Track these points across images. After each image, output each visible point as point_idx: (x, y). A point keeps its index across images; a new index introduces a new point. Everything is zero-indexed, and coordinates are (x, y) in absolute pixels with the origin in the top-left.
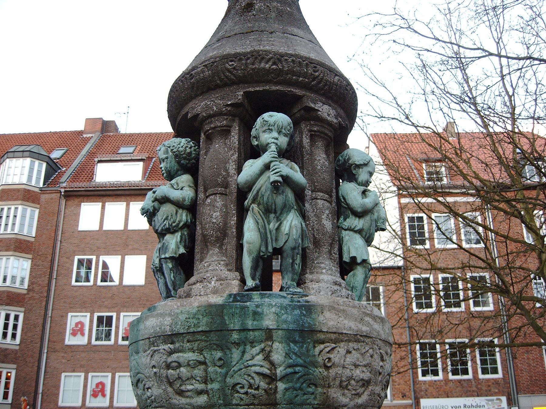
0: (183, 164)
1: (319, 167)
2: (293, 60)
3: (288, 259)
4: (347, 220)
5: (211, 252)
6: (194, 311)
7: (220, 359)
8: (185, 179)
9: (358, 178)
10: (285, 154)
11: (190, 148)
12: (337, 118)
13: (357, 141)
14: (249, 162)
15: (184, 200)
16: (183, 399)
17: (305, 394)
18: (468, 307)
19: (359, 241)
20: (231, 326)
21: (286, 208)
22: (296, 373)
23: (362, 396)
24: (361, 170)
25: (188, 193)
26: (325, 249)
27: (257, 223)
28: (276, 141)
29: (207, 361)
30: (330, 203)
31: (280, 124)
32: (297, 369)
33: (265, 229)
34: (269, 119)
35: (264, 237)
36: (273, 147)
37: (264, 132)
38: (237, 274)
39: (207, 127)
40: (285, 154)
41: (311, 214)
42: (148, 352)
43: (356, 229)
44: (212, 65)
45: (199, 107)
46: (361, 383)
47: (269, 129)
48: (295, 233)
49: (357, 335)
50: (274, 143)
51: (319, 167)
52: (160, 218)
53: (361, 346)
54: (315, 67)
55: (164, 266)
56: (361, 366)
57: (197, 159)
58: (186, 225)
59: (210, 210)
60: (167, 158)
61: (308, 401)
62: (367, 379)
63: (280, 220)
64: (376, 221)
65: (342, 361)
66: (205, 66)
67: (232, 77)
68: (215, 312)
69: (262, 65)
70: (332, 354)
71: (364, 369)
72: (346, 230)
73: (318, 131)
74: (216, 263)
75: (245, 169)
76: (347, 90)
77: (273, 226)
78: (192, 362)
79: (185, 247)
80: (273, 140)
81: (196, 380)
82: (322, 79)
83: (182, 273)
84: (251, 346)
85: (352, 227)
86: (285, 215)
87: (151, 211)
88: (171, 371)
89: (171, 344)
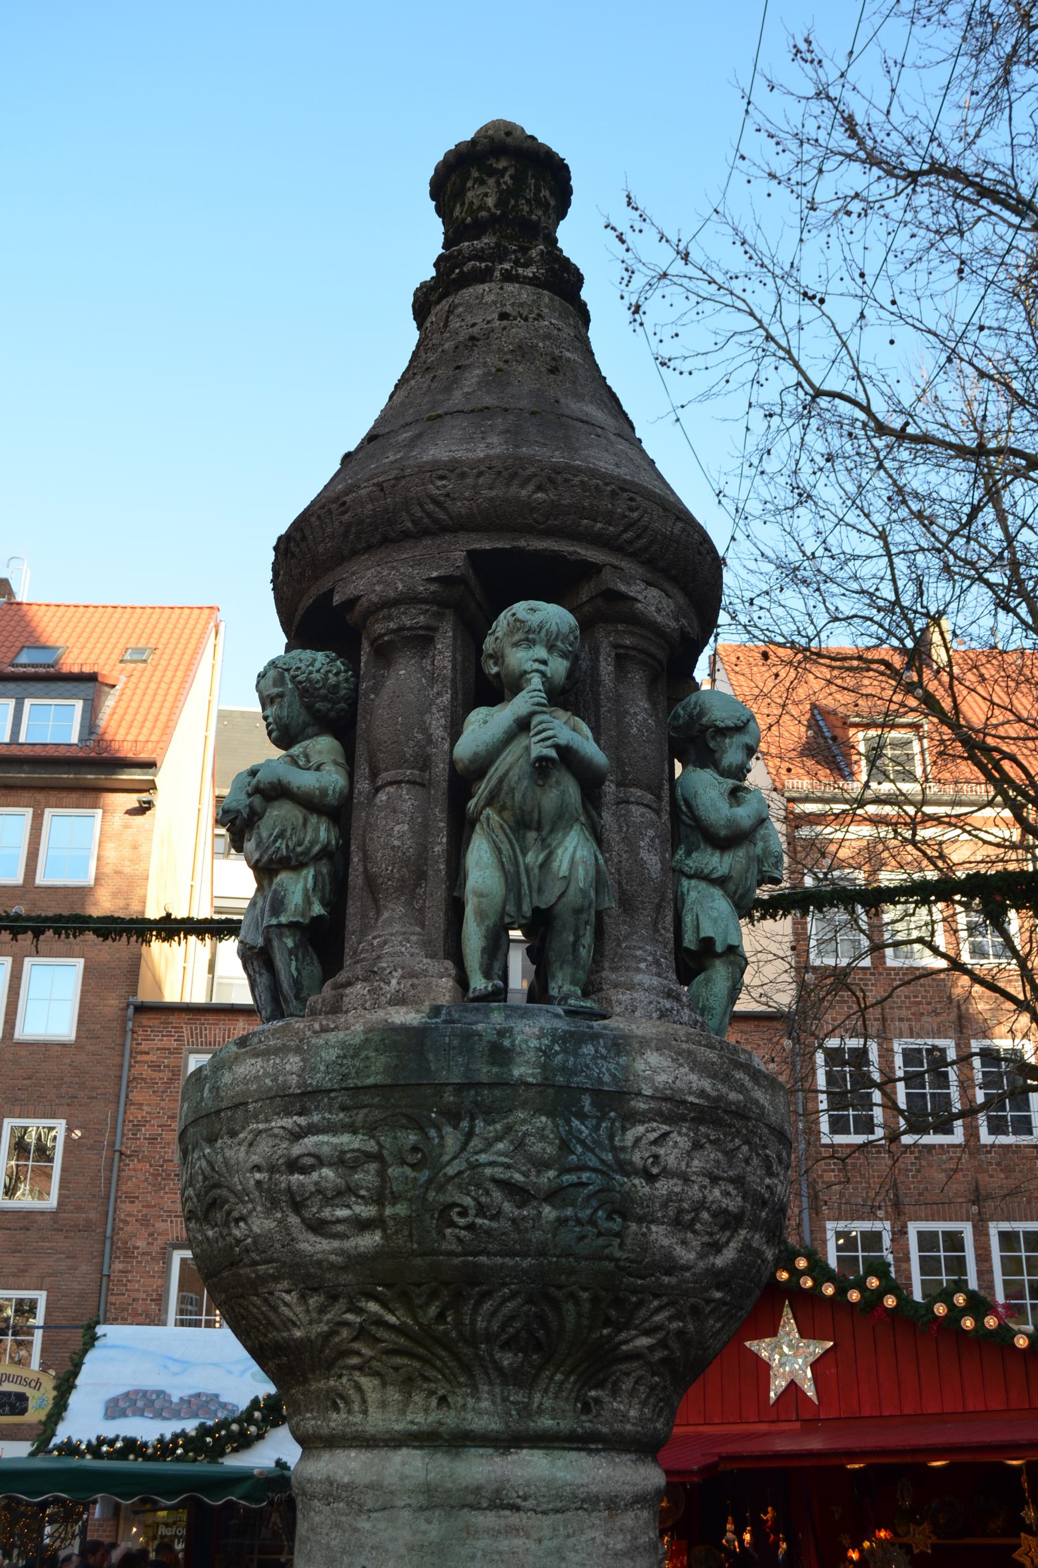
0: (319, 711)
1: (634, 731)
2: (582, 481)
3: (564, 935)
4: (694, 855)
5: (386, 915)
6: (357, 1041)
7: (415, 1149)
8: (323, 746)
9: (720, 759)
10: (561, 696)
11: (337, 674)
12: (677, 620)
13: (724, 670)
14: (478, 715)
15: (324, 792)
16: (325, 1242)
17: (600, 1234)
18: (972, 1133)
19: (720, 904)
20: (443, 1076)
21: (561, 821)
22: (585, 1185)
23: (725, 1251)
24: (727, 741)
25: (331, 779)
26: (645, 917)
27: (499, 851)
28: (542, 667)
29: (385, 1152)
30: (657, 812)
31: (554, 628)
32: (585, 1176)
33: (517, 864)
34: (529, 617)
35: (512, 880)
36: (536, 681)
37: (516, 645)
38: (449, 964)
39: (379, 628)
40: (561, 696)
41: (613, 836)
42: (242, 1136)
43: (715, 876)
44: (394, 486)
45: (366, 580)
46: (721, 1220)
47: (527, 639)
48: (582, 876)
49: (717, 1108)
50: (537, 671)
51: (634, 731)
52: (265, 834)
53: (725, 1135)
54: (631, 499)
55: (275, 944)
56: (724, 1179)
57: (353, 700)
58: (326, 853)
59: (385, 818)
60: (281, 695)
61: (607, 1251)
62: (736, 1210)
63: (549, 845)
64: (760, 861)
65: (683, 1164)
66: (380, 485)
67: (442, 516)
68: (408, 1044)
69: (514, 489)
70: (662, 1146)
71: (731, 1188)
72: (690, 877)
73: (634, 648)
74: (400, 938)
75: (471, 728)
76: (700, 553)
77: (533, 858)
78: (348, 1156)
79: (323, 903)
80: (536, 666)
81: (358, 1196)
82: (646, 528)
83: (316, 961)
84: (485, 1121)
85: (706, 871)
86: (560, 835)
87: (245, 815)
88: (297, 1178)
89: (300, 1114)
